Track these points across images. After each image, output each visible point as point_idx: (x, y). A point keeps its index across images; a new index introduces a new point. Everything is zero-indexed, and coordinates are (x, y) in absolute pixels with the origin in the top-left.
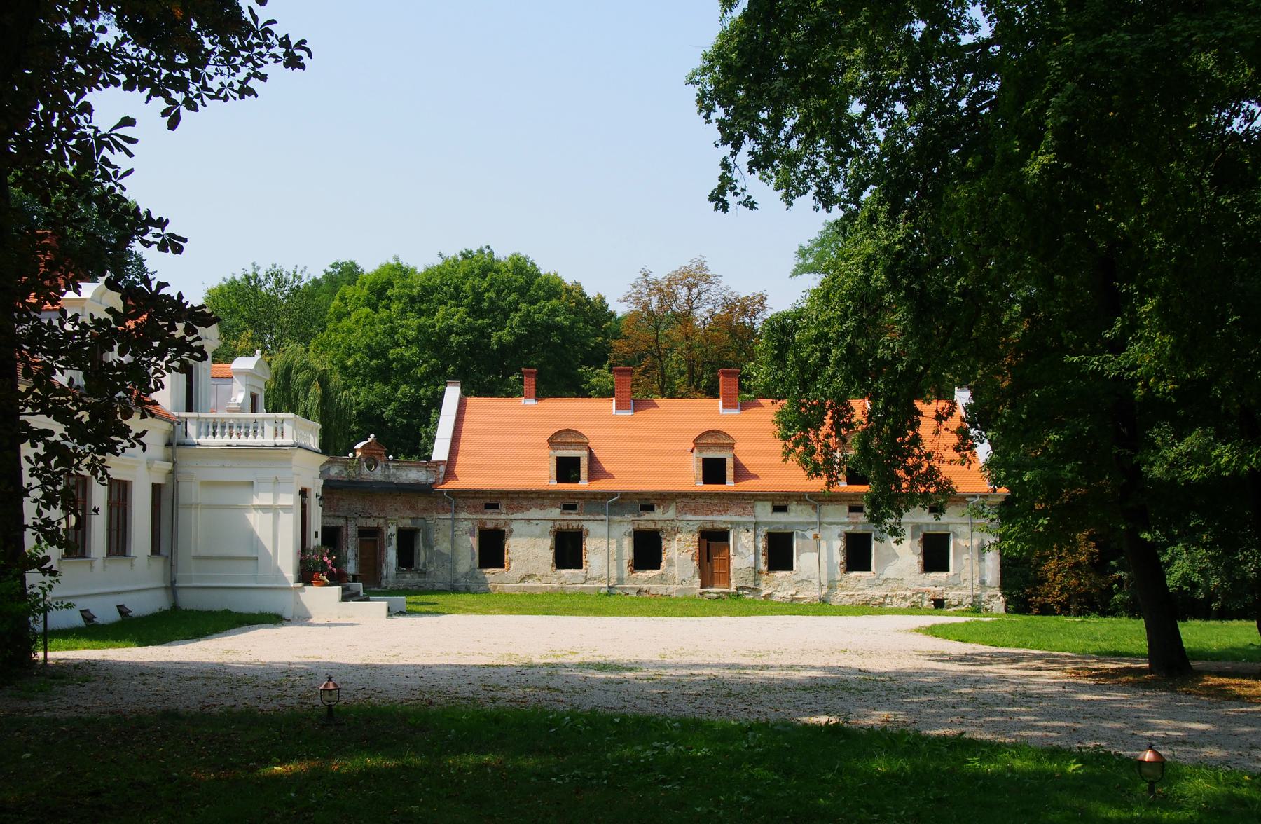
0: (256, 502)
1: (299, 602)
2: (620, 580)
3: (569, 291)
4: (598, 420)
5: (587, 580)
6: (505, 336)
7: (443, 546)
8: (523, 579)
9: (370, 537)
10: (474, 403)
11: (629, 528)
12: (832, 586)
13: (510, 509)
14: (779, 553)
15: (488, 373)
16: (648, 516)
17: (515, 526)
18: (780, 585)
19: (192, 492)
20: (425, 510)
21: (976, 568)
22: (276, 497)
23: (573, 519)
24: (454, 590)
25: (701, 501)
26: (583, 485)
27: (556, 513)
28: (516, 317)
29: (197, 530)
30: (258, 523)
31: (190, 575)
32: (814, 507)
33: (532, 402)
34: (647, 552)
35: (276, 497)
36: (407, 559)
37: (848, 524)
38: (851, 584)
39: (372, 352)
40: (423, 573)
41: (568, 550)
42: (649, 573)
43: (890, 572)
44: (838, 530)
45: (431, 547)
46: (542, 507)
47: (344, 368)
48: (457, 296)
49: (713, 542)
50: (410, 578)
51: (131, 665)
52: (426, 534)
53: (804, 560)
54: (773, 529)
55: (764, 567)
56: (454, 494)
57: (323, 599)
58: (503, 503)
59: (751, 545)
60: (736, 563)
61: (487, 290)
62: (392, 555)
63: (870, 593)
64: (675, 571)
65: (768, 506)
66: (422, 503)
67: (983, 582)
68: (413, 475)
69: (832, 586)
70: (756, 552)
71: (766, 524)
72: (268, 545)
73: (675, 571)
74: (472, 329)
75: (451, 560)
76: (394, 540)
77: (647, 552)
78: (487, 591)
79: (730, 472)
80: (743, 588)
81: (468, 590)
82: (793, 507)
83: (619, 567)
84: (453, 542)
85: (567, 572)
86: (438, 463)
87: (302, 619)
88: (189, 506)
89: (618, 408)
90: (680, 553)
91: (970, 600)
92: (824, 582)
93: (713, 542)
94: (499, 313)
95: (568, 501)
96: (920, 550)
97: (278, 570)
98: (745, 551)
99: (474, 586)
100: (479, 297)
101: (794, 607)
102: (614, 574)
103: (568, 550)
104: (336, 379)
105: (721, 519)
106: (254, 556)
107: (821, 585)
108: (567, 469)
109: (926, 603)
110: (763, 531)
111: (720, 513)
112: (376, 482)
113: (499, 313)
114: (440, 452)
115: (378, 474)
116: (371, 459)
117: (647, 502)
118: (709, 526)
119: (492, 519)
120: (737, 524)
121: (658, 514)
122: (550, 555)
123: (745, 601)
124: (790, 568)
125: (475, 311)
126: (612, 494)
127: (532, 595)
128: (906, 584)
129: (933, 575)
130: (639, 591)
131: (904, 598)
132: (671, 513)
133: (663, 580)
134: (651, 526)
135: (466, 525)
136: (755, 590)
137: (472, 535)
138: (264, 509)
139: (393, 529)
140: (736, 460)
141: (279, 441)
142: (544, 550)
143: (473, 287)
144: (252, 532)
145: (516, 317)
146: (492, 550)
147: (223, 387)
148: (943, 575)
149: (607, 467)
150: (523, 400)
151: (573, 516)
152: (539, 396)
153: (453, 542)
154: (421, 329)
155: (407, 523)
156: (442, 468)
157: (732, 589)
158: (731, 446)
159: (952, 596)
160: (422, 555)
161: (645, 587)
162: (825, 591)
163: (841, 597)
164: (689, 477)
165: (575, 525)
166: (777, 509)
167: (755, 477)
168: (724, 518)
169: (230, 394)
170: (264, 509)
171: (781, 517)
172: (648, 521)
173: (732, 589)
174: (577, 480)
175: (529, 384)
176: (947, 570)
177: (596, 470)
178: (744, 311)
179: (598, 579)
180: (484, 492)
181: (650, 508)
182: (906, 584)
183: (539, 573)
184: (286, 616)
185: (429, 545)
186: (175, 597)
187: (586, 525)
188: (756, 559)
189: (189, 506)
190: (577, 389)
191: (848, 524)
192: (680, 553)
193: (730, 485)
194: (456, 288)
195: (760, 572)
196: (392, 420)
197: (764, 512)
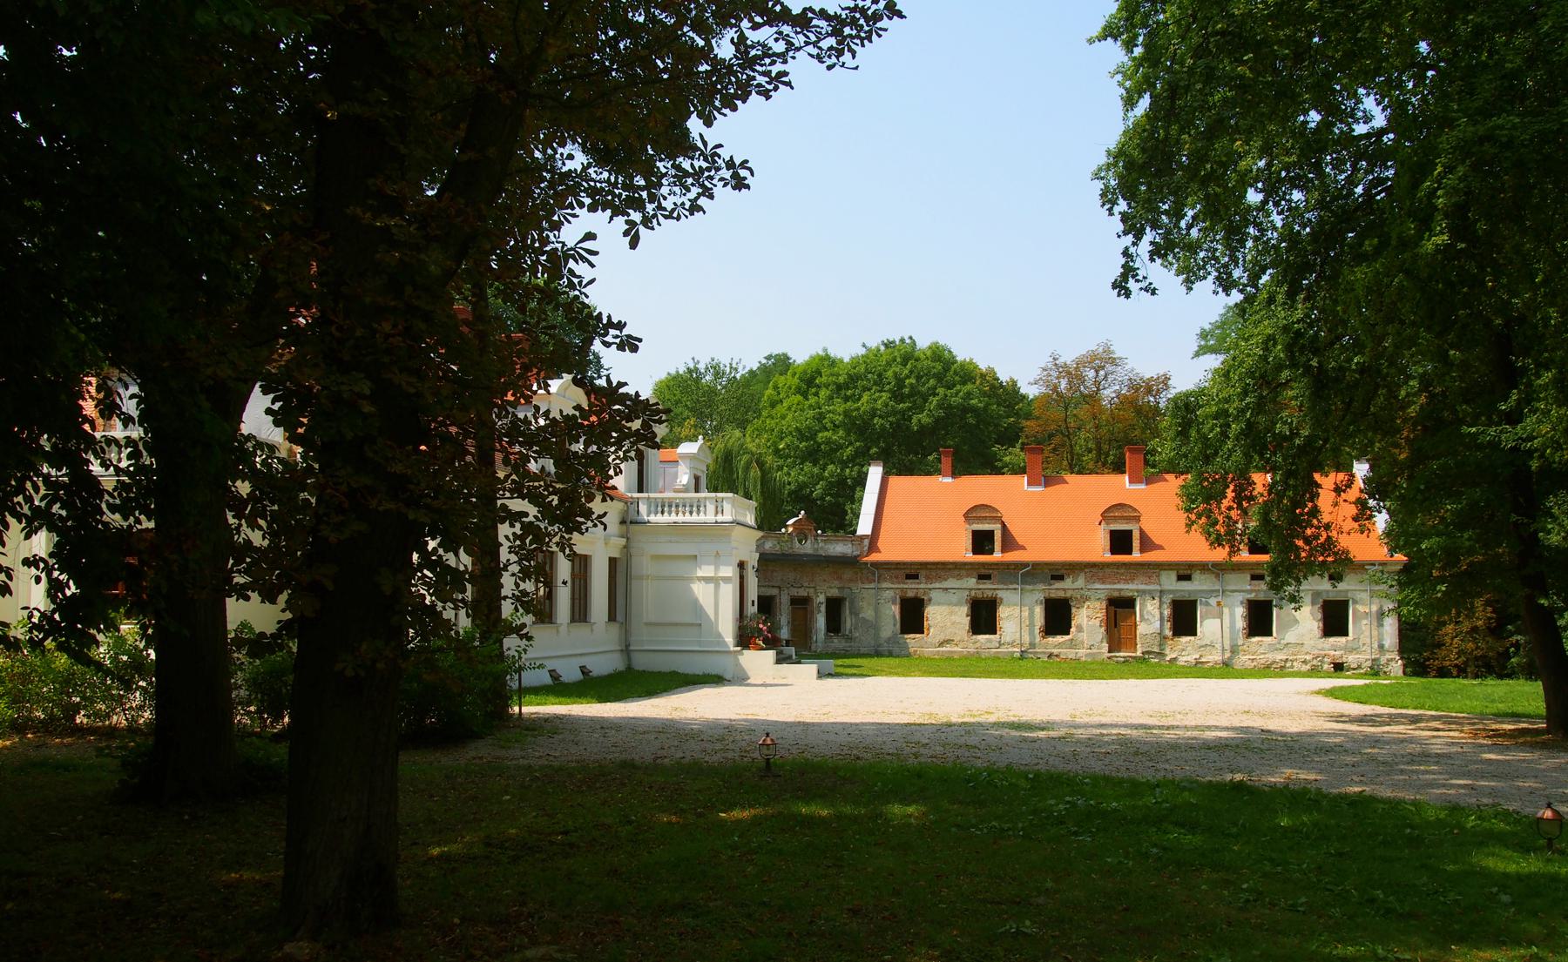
0: (700, 573)
1: (738, 665)
2: (1032, 645)
3: (983, 376)
4: (1012, 495)
5: (1001, 644)
6: (924, 418)
7: (868, 613)
8: (941, 644)
9: (801, 604)
10: (895, 481)
11: (1041, 597)
12: (1234, 650)
13: (929, 579)
14: (1183, 619)
15: (908, 452)
16: (1058, 585)
17: (933, 594)
18: (1184, 649)
19: (643, 565)
20: (851, 580)
21: (1375, 633)
22: (717, 569)
23: (987, 589)
24: (878, 654)
25: (1108, 571)
26: (997, 556)
27: (972, 582)
28: (934, 400)
29: (648, 598)
30: (702, 592)
31: (643, 639)
32: (1217, 576)
33: (949, 480)
34: (1058, 618)
35: (717, 569)
36: (834, 625)
37: (1250, 592)
38: (1253, 648)
39: (800, 435)
40: (849, 639)
41: (983, 617)
42: (1060, 639)
43: (1291, 636)
44: (1240, 597)
45: (857, 615)
46: (959, 577)
47: (777, 452)
48: (880, 381)
49: (1120, 609)
50: (837, 643)
51: (592, 719)
52: (852, 603)
53: (1208, 627)
54: (1178, 597)
55: (1168, 633)
56: (876, 565)
57: (759, 661)
58: (922, 573)
59: (1157, 613)
60: (1142, 629)
61: (908, 377)
62: (821, 621)
63: (1271, 657)
64: (1084, 636)
65: (1173, 575)
66: (848, 574)
67: (1381, 647)
68: (840, 548)
69: (1234, 650)
70: (1162, 619)
71: (1171, 592)
72: (710, 612)
73: (1084, 636)
74: (894, 412)
75: (875, 626)
76: (823, 608)
77: (1058, 618)
78: (908, 655)
79: (1136, 543)
80: (1149, 653)
81: (890, 654)
82: (1197, 576)
83: (1031, 633)
84: (877, 611)
85: (982, 638)
86: (862, 537)
87: (741, 679)
88: (641, 578)
89: (1029, 484)
90: (1088, 620)
91: (1369, 663)
92: (1227, 647)
93: (1120, 609)
94: (919, 398)
95: (983, 572)
96: (1320, 616)
97: (720, 635)
98: (1150, 618)
99: (896, 650)
100: (900, 382)
101: (1199, 670)
102: (1026, 639)
103: (983, 617)
104: (769, 459)
105: (1127, 588)
106: (698, 622)
107: (1223, 650)
108: (982, 542)
109: (1326, 667)
110: (1168, 599)
111: (1126, 581)
112: (806, 555)
113: (919, 398)
114: (864, 527)
115: (808, 547)
116: (801, 533)
117: (1057, 572)
118: (1116, 594)
119: (912, 588)
120: (1144, 592)
121: (1068, 583)
122: (966, 621)
123: (1151, 665)
124: (1195, 634)
125: (897, 396)
126: (1025, 565)
127: (949, 658)
128: (1306, 648)
129: (1332, 640)
130: (1050, 655)
131: (1305, 662)
132: (1080, 582)
133: (1072, 644)
134: (1061, 594)
135: (888, 594)
136: (1161, 654)
137: (894, 603)
138: (707, 580)
139: (822, 598)
140: (1142, 532)
141: (720, 518)
142: (962, 616)
143: (895, 373)
144: (696, 600)
145: (934, 400)
146: (912, 617)
147: (670, 470)
148: (1342, 640)
149: (1020, 540)
150: (940, 478)
151: (987, 585)
152: (955, 474)
153: (877, 611)
154: (846, 413)
155: (834, 592)
156: (866, 542)
157: (1139, 653)
158: (1137, 519)
159: (1351, 659)
160: (848, 622)
161: (1055, 651)
162: (1228, 655)
163: (1243, 660)
164: (1097, 548)
165: (990, 593)
166: (1181, 578)
167: (1160, 547)
168: (1130, 586)
169: (676, 476)
170: (707, 580)
171: (1185, 586)
172: (1059, 589)
173: (1139, 653)
174: (991, 552)
175: (946, 463)
176: (1270, 634)
177: (1009, 543)
178: (1149, 391)
179: (1012, 644)
180: (904, 563)
181: (1061, 578)
182: (1306, 648)
183: (956, 639)
184: (728, 677)
185: (854, 613)
186: (629, 659)
187: (1000, 594)
188: (1162, 625)
189: (641, 578)
190: (991, 466)
191: (1250, 592)
192: (1088, 620)
193: (1136, 556)
194: (880, 375)
195: (1165, 638)
196: (822, 499)
197: (1169, 581)
